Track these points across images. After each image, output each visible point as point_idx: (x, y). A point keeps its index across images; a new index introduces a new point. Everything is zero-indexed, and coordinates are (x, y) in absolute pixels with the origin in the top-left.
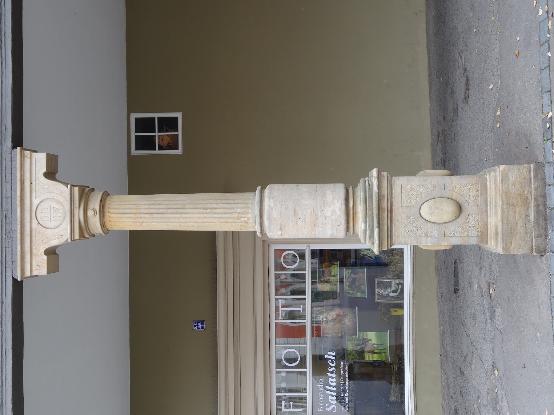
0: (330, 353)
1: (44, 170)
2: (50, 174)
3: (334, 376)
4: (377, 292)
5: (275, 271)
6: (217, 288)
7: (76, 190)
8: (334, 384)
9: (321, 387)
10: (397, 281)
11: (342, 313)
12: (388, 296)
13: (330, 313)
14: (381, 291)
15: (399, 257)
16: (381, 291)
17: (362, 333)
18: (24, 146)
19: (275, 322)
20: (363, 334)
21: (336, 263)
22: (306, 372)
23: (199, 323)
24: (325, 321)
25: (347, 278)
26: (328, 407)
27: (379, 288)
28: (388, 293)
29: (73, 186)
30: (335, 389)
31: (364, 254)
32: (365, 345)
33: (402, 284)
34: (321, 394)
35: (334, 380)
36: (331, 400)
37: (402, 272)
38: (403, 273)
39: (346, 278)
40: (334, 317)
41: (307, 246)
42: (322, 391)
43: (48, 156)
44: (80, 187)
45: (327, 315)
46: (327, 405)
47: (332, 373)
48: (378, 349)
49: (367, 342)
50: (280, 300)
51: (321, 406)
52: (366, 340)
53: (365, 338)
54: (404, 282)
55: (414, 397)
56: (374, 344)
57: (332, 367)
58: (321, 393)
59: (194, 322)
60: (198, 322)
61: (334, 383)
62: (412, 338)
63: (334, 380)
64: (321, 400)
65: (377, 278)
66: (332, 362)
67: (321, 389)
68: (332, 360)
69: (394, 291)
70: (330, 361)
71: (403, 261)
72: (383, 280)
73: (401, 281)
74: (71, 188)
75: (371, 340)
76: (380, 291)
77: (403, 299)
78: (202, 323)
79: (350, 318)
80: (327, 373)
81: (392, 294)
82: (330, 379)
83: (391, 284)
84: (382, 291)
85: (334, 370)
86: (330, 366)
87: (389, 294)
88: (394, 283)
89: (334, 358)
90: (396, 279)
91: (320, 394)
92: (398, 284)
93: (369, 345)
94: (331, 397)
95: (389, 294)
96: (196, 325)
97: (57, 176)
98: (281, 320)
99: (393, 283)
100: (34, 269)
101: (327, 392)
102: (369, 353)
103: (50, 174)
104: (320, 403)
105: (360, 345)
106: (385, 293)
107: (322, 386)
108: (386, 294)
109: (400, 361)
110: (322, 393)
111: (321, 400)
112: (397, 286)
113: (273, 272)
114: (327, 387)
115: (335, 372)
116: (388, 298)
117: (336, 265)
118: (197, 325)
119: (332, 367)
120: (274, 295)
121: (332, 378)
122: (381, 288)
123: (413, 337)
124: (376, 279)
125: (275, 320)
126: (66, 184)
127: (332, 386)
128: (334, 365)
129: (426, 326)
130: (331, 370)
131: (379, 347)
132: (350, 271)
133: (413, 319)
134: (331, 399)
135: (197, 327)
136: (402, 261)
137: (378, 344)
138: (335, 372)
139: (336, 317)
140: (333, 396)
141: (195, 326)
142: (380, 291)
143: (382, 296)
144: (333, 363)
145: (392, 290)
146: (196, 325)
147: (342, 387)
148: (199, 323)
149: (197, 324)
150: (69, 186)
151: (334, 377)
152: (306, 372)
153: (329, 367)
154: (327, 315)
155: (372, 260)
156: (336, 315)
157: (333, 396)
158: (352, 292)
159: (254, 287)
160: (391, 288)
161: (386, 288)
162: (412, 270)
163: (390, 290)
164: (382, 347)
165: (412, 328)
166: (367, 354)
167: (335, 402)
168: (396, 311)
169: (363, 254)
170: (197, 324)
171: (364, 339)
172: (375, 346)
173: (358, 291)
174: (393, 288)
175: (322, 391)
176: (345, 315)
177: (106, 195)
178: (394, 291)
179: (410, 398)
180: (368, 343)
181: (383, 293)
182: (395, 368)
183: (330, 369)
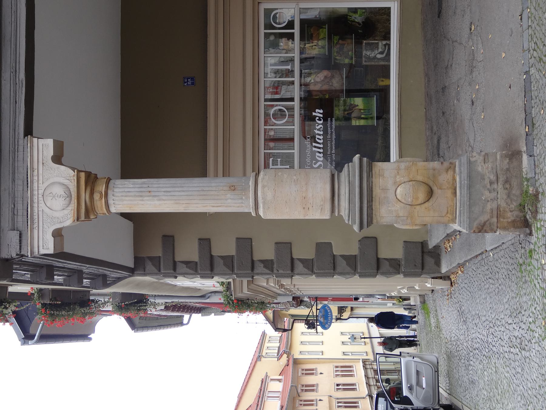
0: (317, 110)
1: (52, 153)
2: (57, 159)
3: (322, 133)
4: (364, 54)
5: (264, 30)
6: (208, 39)
7: (83, 175)
8: (321, 141)
9: (308, 144)
10: (384, 42)
11: (330, 74)
12: (375, 58)
13: (319, 75)
14: (368, 53)
15: (386, 16)
16: (368, 53)
17: (349, 98)
18: (34, 135)
19: (264, 128)
20: (350, 100)
21: (324, 27)
22: (293, 34)
23: (189, 79)
24: (313, 82)
25: (335, 44)
26: (315, 164)
27: (366, 50)
28: (375, 55)
29: (79, 171)
30: (321, 146)
31: (352, 19)
32: (351, 111)
33: (389, 45)
34: (308, 151)
35: (321, 137)
36: (318, 156)
37: (389, 33)
38: (390, 34)
39: (334, 44)
40: (322, 78)
41: (296, 5)
42: (309, 148)
43: (55, 142)
44: (85, 172)
45: (315, 77)
46: (314, 162)
47: (319, 130)
48: (364, 114)
49: (353, 107)
50: (269, 59)
51: (308, 163)
52: (353, 106)
53: (352, 103)
54: (390, 42)
55: (399, 150)
56: (361, 110)
57: (319, 124)
58: (308, 150)
59: (184, 78)
60: (188, 79)
61: (321, 140)
62: (398, 76)
63: (321, 137)
64: (309, 157)
65: (365, 40)
66: (320, 120)
67: (309, 146)
68: (320, 117)
69: (382, 53)
70: (318, 118)
71: (390, 20)
72: (370, 42)
73: (388, 42)
74: (78, 173)
75: (358, 106)
76: (366, 53)
77: (389, 60)
78: (192, 79)
79: (338, 80)
80: (314, 130)
81: (379, 56)
82: (317, 136)
83: (378, 45)
84: (369, 53)
85: (321, 128)
86: (317, 123)
87: (376, 55)
88: (381, 44)
89: (321, 116)
90: (383, 39)
91: (307, 151)
92: (385, 45)
93: (355, 110)
94: (318, 154)
95: (376, 55)
96: (186, 81)
97: (63, 160)
98: (270, 78)
99: (380, 44)
100: (41, 248)
101: (314, 149)
102: (356, 119)
103: (57, 159)
104: (307, 160)
105: (347, 111)
106: (373, 55)
107: (310, 143)
108: (373, 56)
109: (386, 123)
110: (309, 150)
111: (309, 157)
112: (383, 47)
113: (262, 31)
114: (314, 144)
115: (322, 129)
116: (376, 60)
117: (324, 28)
118: (188, 81)
119: (319, 124)
120: (264, 101)
121: (319, 135)
122: (368, 50)
123: (399, 91)
124: (363, 41)
125: (264, 78)
126: (73, 169)
127: (319, 143)
128: (322, 122)
129: (412, 81)
130: (318, 128)
131: (365, 112)
132: (339, 38)
133: (399, 73)
134: (318, 156)
135: (187, 83)
136: (389, 20)
137: (364, 109)
138: (322, 129)
139: (324, 79)
140: (320, 153)
141: (185, 82)
142: (366, 53)
143: (369, 59)
144: (321, 120)
145: (379, 51)
146: (186, 81)
147: (329, 144)
148: (189, 79)
149: (188, 80)
150: (76, 171)
151: (321, 152)
152: (293, 34)
153: (317, 125)
154: (315, 77)
155: (359, 26)
156: (324, 77)
157: (320, 153)
158: (339, 58)
159: (244, 41)
160: (378, 49)
161: (372, 50)
162: (399, 21)
163: (377, 52)
164: (368, 112)
165: (398, 82)
166: (354, 120)
167: (322, 159)
168: (383, 81)
169: (351, 20)
170: (188, 80)
171: (351, 105)
172: (362, 111)
173: (346, 57)
174: (380, 50)
175: (309, 148)
176: (333, 77)
177: (109, 180)
178: (382, 53)
179: (395, 147)
180: (355, 108)
181: (371, 56)
182: (380, 130)
183: (317, 126)
